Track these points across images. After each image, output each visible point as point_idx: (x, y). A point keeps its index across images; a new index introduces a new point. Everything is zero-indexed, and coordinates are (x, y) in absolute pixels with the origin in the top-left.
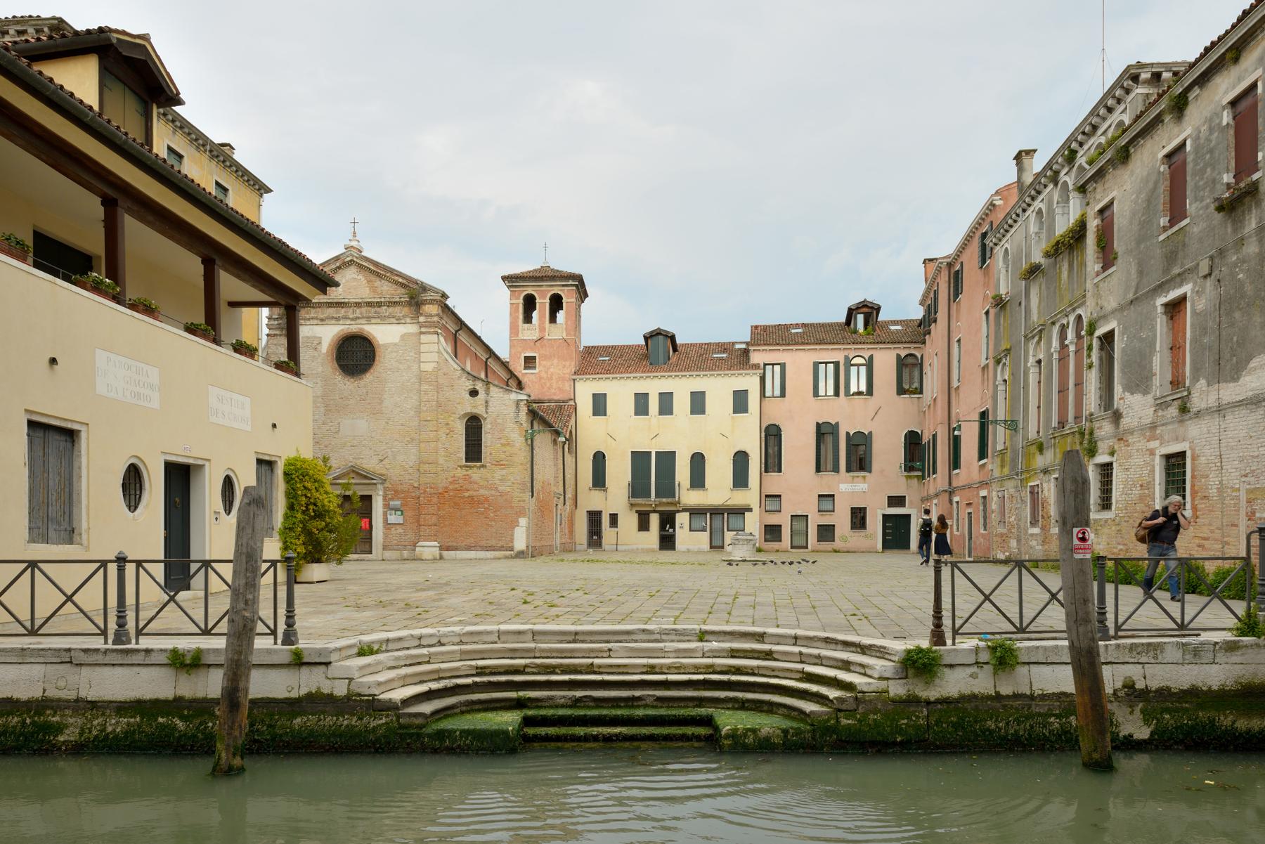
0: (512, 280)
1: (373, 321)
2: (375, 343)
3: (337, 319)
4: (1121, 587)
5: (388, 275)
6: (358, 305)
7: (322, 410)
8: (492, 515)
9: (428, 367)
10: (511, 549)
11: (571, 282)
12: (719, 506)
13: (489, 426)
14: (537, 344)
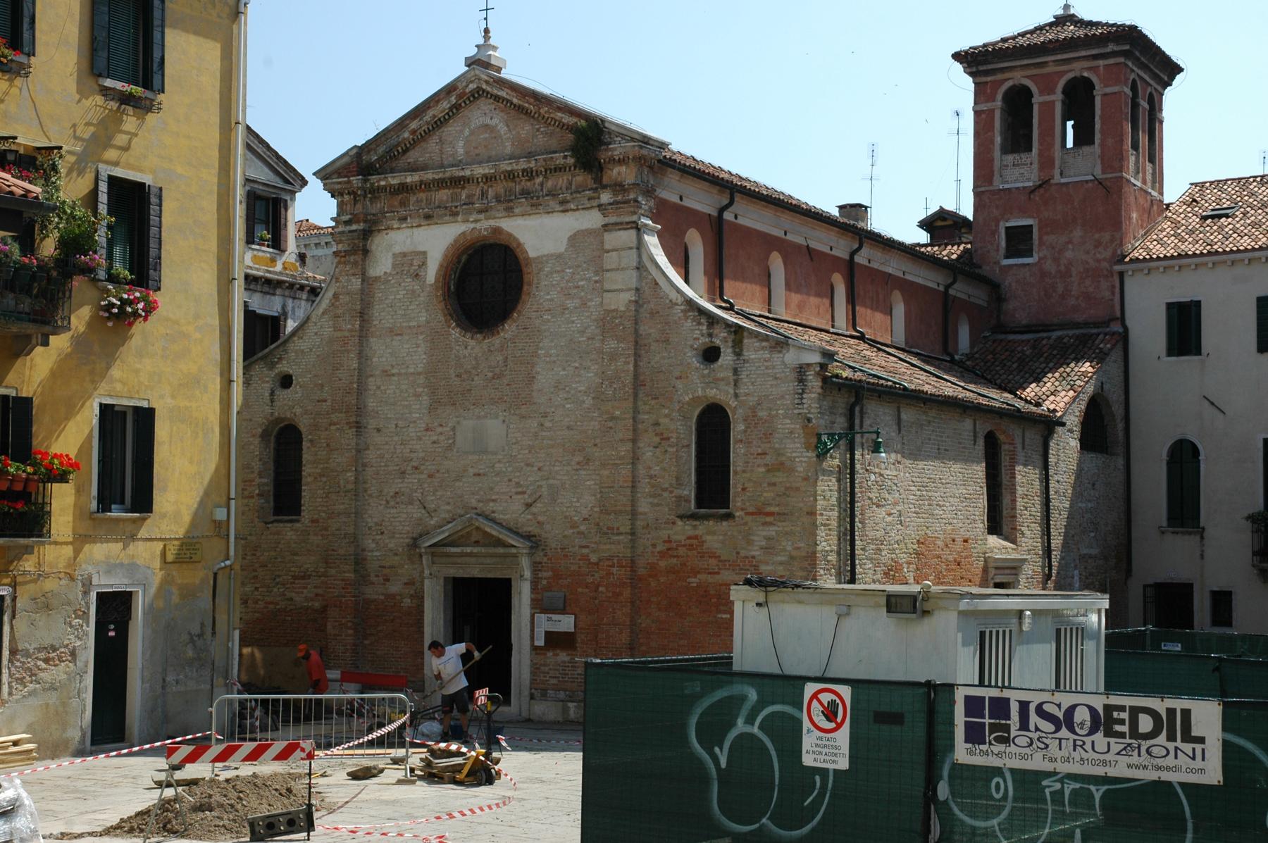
0: (973, 60)
7: (425, 399)
11: (1111, 47)
13: (741, 427)
14: (1036, 197)
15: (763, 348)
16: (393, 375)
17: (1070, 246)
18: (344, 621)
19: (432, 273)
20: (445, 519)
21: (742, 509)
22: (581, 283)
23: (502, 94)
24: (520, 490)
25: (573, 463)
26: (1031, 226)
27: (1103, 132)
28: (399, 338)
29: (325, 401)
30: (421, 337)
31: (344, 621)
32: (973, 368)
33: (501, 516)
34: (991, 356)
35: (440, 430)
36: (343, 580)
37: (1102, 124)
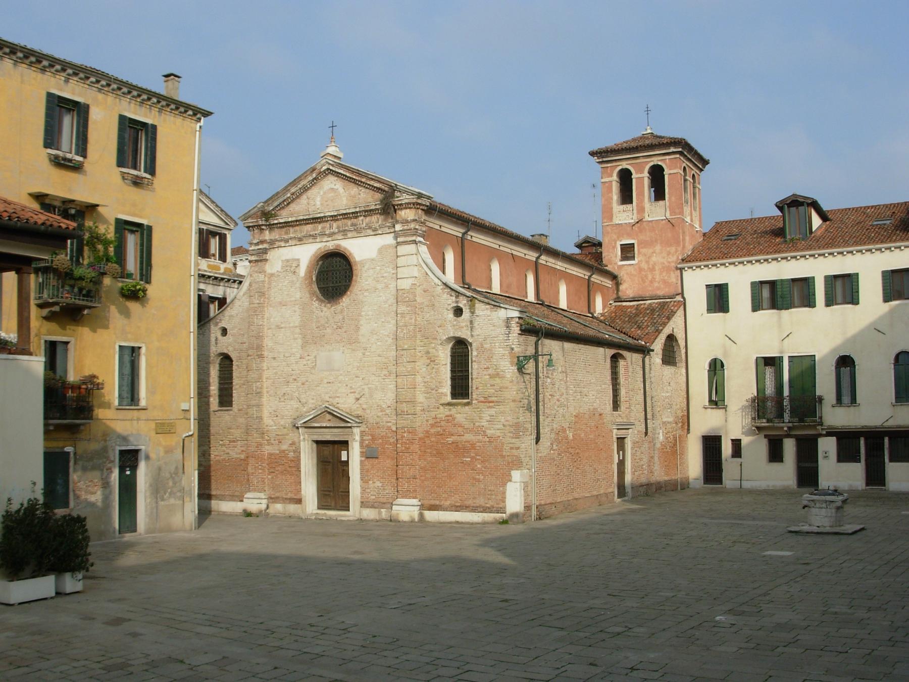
1: (350, 235)
2: (352, 260)
3: (314, 237)
5: (363, 180)
6: (334, 218)
7: (300, 341)
8: (479, 466)
9: (405, 284)
10: (502, 510)
11: (672, 149)
12: (876, 427)
15: (487, 309)
16: (282, 328)
17: (655, 255)
18: (257, 465)
19: (302, 271)
20: (311, 408)
21: (476, 400)
22: (385, 275)
23: (341, 172)
24: (352, 391)
25: (382, 375)
26: (633, 244)
27: (669, 194)
28: (285, 307)
29: (245, 343)
30: (297, 306)
31: (257, 465)
32: (604, 320)
33: (343, 406)
34: (614, 314)
35: (307, 358)
36: (256, 443)
37: (669, 189)
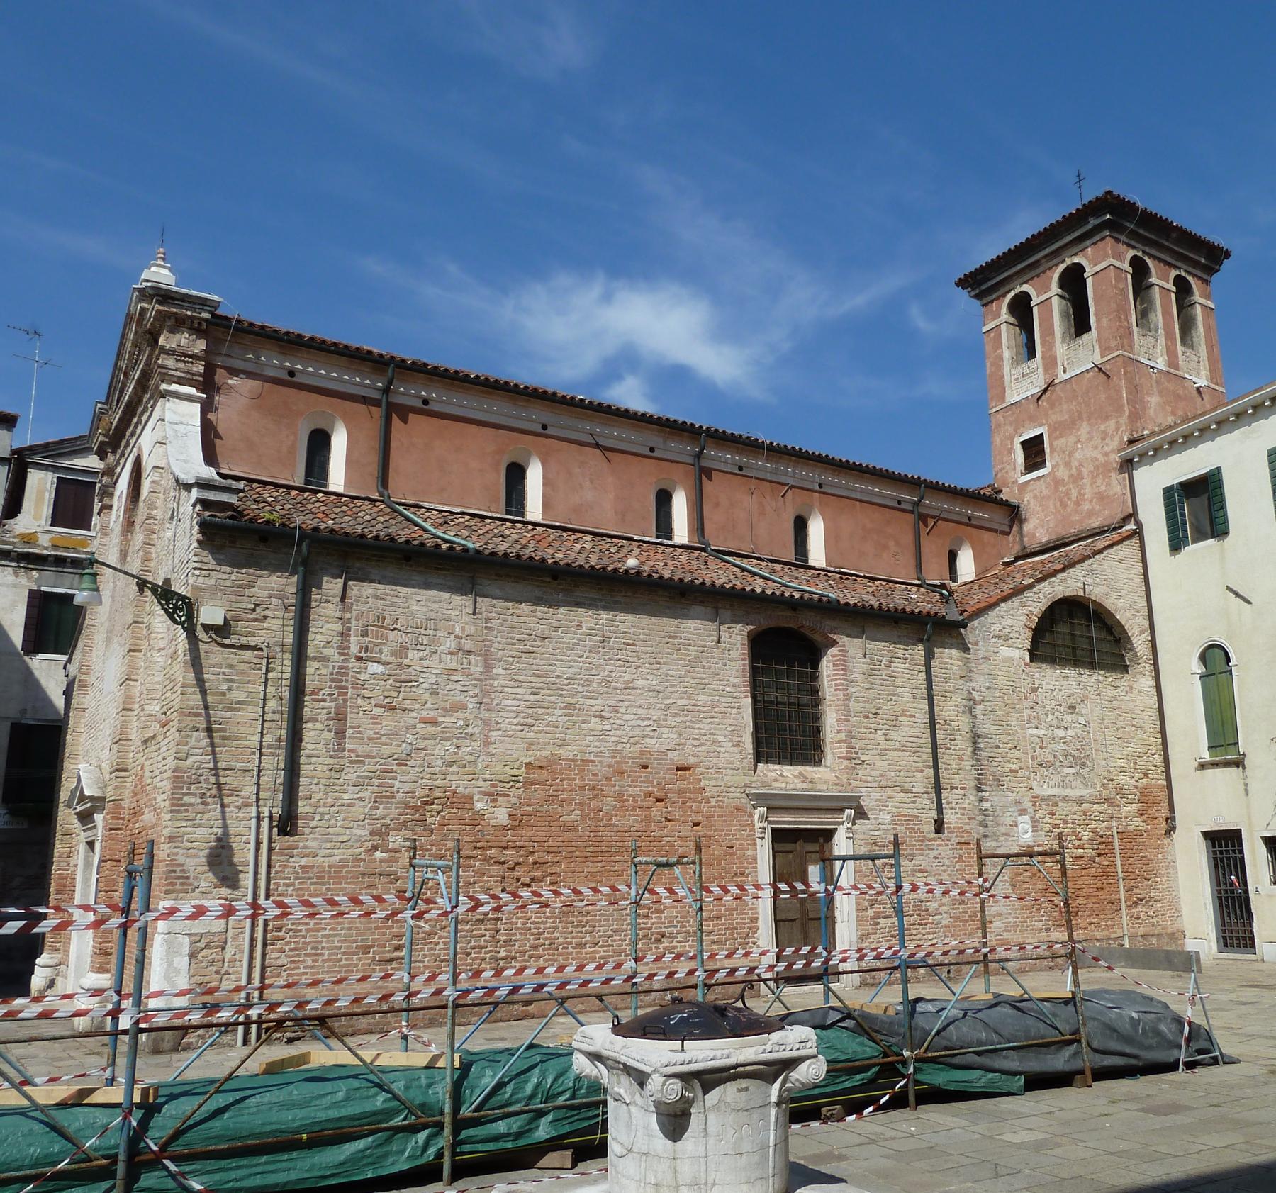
4: (480, 599)
11: (1093, 222)
